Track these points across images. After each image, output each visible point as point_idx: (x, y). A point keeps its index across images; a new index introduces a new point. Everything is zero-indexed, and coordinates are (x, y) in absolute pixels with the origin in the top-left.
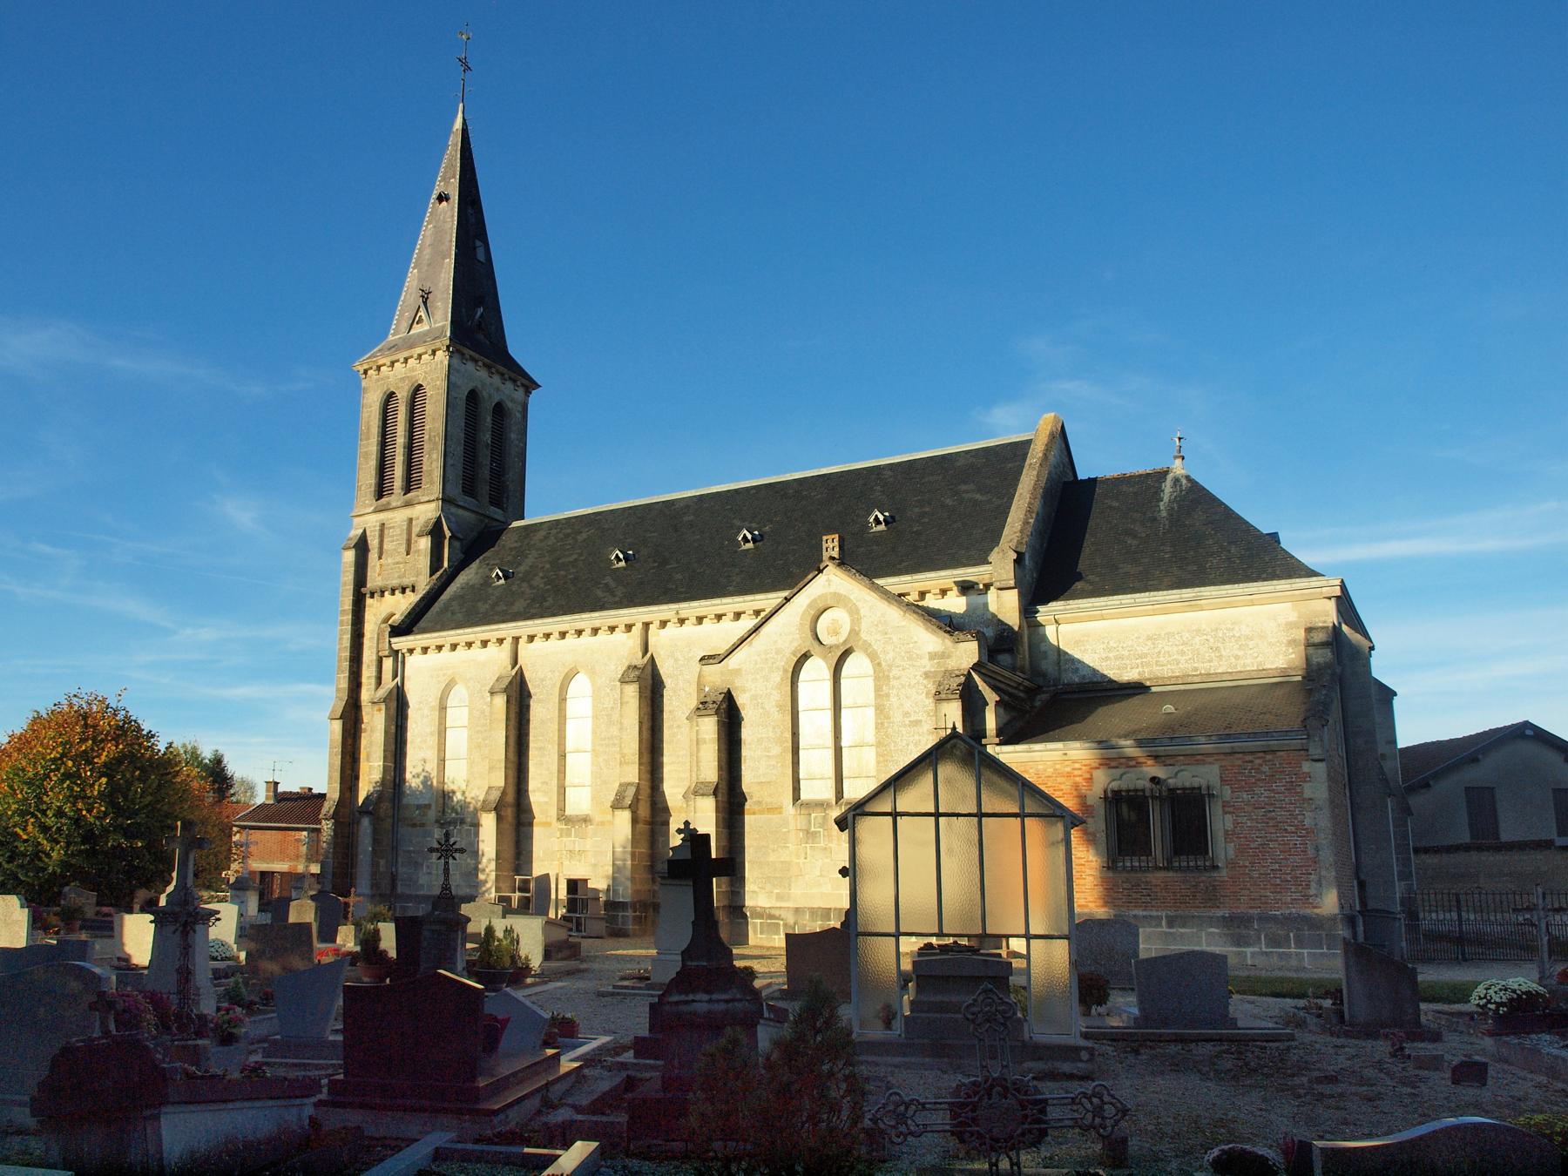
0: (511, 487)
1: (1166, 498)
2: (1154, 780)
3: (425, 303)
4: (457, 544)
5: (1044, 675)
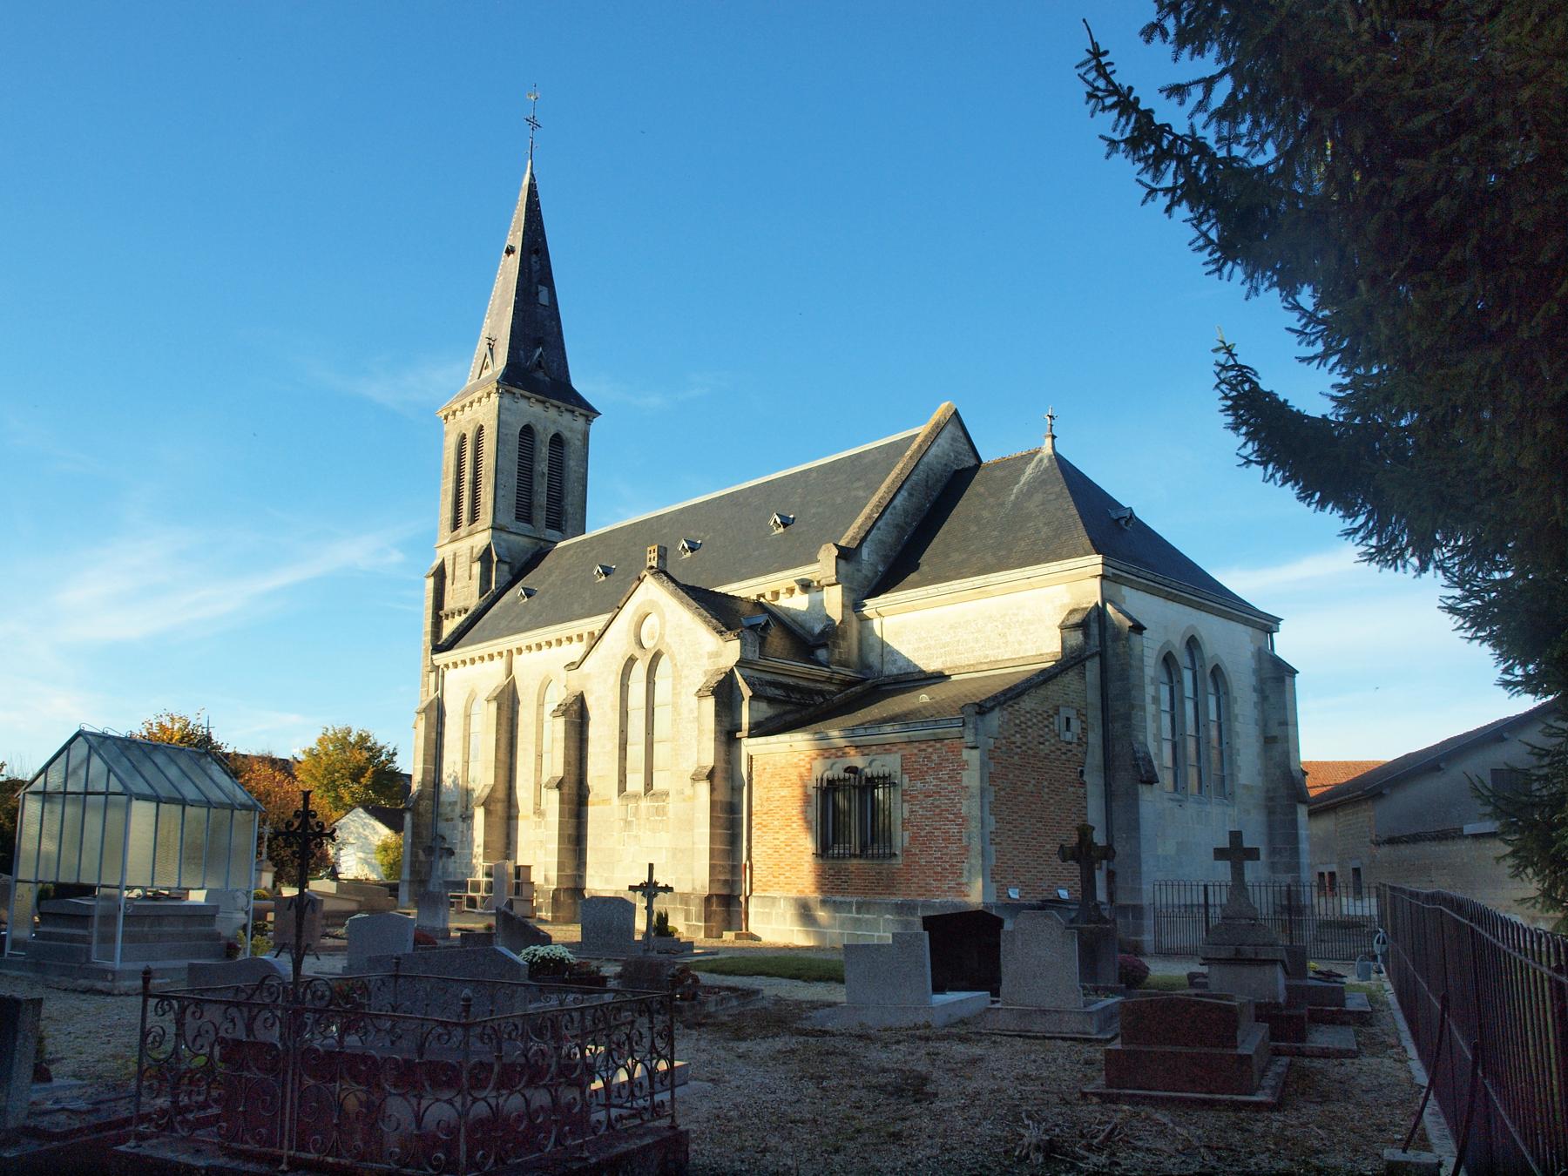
0: (570, 510)
1: (1023, 480)
2: (852, 770)
4: (505, 568)
5: (870, 667)
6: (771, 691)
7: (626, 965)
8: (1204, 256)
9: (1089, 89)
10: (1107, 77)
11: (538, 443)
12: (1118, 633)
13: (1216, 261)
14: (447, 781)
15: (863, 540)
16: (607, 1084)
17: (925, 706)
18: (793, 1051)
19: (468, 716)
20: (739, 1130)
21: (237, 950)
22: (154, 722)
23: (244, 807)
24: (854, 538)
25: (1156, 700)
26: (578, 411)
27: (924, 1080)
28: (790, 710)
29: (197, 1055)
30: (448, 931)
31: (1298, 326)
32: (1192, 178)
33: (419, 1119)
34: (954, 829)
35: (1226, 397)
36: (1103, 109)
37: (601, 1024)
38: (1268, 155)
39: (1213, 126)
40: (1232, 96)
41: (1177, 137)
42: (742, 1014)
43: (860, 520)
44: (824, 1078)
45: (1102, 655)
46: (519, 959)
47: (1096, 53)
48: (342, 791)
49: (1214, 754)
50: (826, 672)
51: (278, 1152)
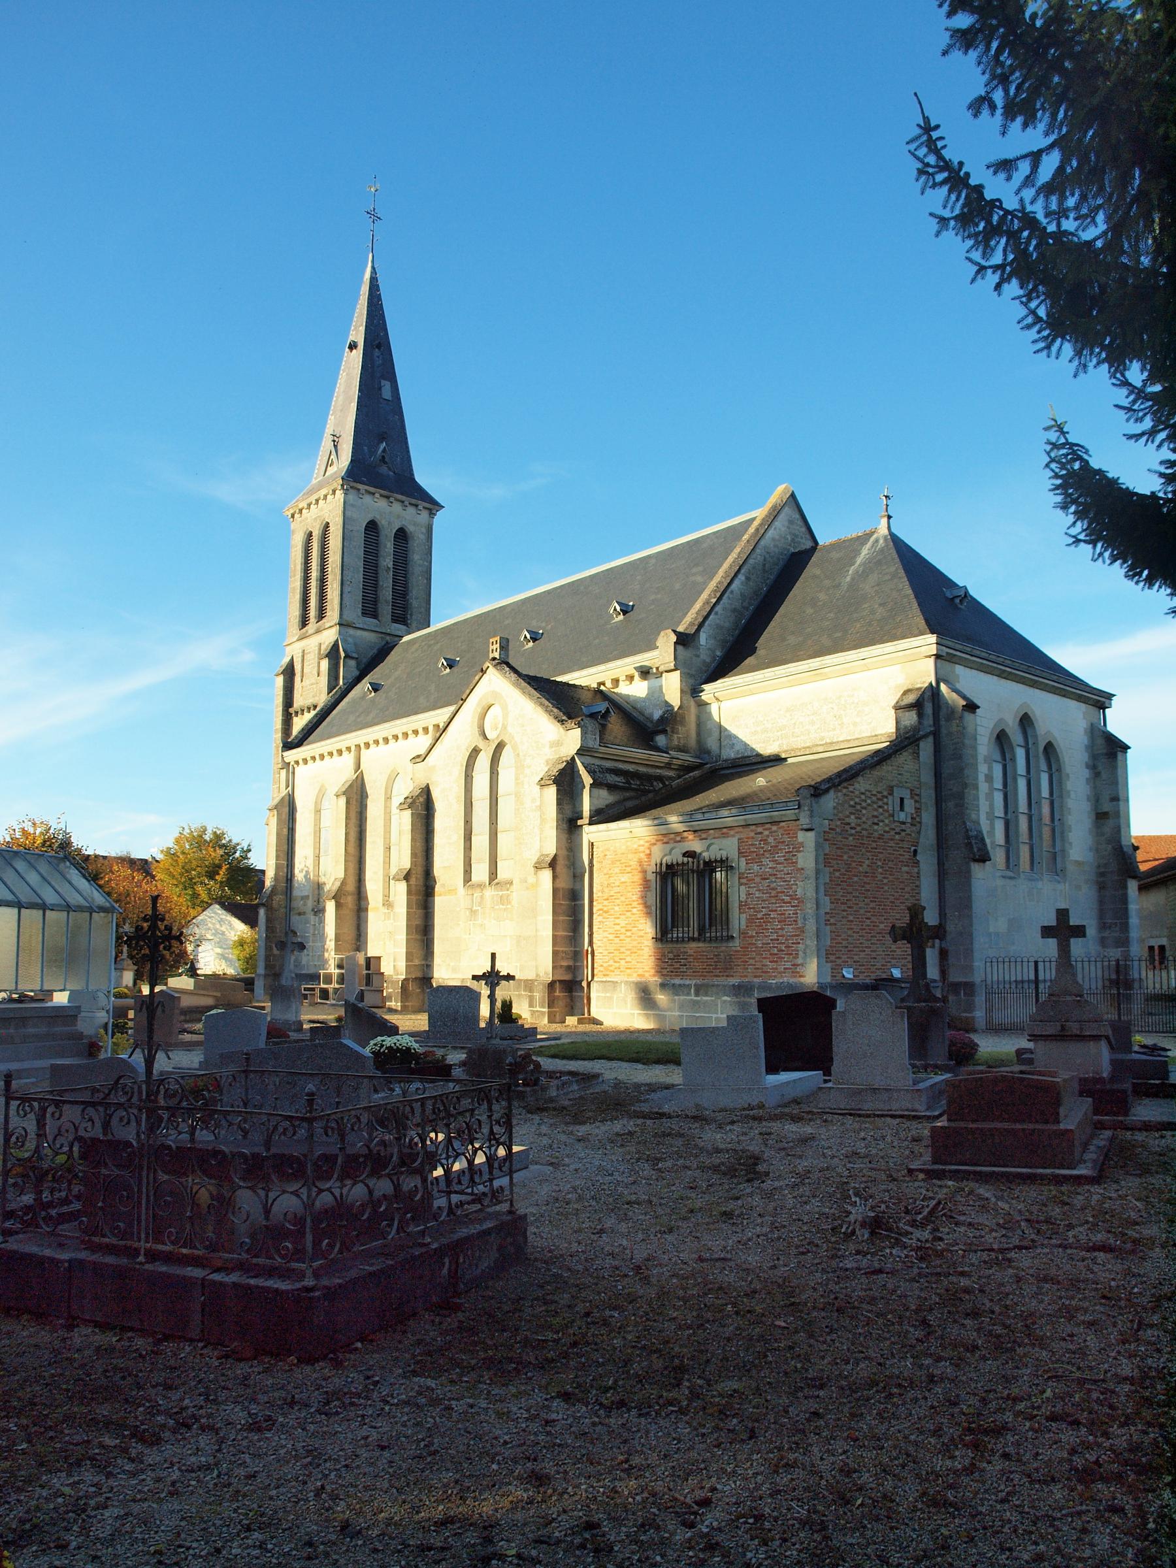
0: (415, 603)
1: (859, 560)
2: (689, 854)
3: (335, 446)
4: (352, 663)
5: (708, 752)
6: (612, 779)
7: (470, 1052)
8: (1033, 334)
9: (920, 165)
10: (937, 152)
11: (382, 538)
12: (952, 711)
13: (1045, 338)
14: (299, 876)
15: (701, 625)
16: (448, 1171)
17: (762, 789)
18: (630, 1133)
19: (318, 812)
20: (577, 1212)
21: (99, 1048)
22: (17, 828)
23: (102, 909)
24: (691, 624)
25: (989, 778)
26: (422, 504)
27: (756, 1159)
28: (631, 796)
29: (57, 1154)
30: (300, 1023)
31: (1125, 403)
32: (1022, 254)
33: (267, 1211)
34: (790, 910)
35: (1056, 476)
36: (934, 185)
37: (441, 1113)
38: (1094, 231)
39: (1041, 201)
40: (1060, 170)
41: (1007, 212)
42: (581, 1098)
43: (698, 605)
44: (660, 1160)
45: (936, 734)
46: (366, 1052)
47: (928, 128)
48: (199, 889)
49: (1046, 831)
50: (664, 758)
51: (136, 1245)
